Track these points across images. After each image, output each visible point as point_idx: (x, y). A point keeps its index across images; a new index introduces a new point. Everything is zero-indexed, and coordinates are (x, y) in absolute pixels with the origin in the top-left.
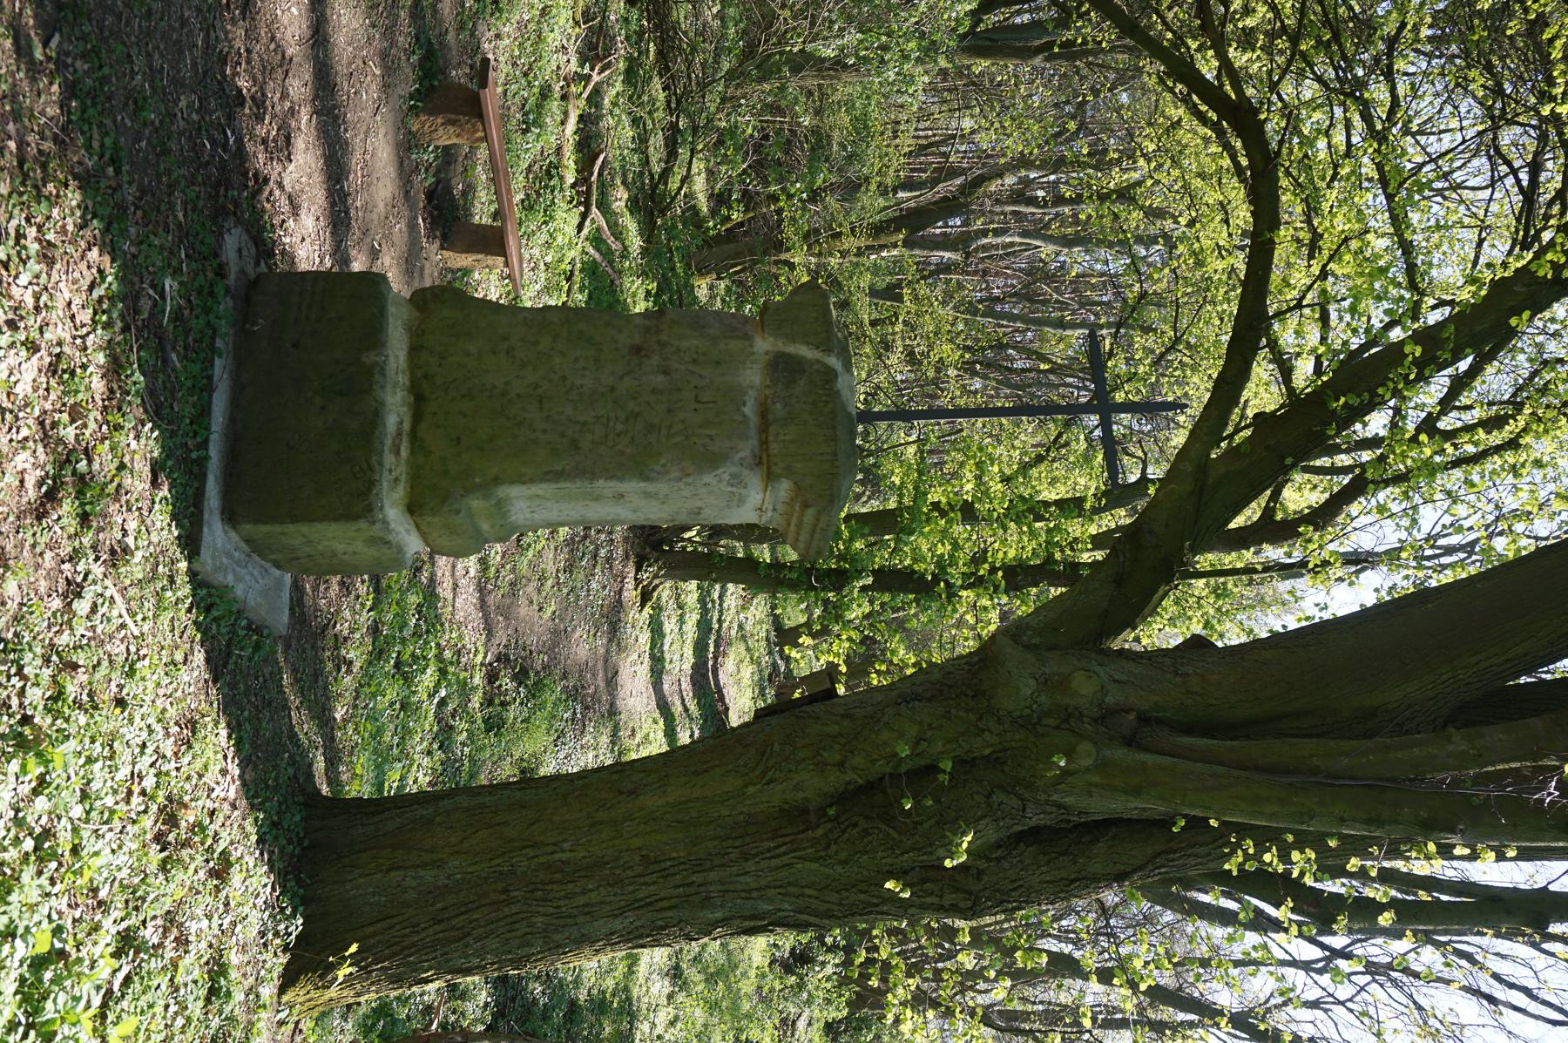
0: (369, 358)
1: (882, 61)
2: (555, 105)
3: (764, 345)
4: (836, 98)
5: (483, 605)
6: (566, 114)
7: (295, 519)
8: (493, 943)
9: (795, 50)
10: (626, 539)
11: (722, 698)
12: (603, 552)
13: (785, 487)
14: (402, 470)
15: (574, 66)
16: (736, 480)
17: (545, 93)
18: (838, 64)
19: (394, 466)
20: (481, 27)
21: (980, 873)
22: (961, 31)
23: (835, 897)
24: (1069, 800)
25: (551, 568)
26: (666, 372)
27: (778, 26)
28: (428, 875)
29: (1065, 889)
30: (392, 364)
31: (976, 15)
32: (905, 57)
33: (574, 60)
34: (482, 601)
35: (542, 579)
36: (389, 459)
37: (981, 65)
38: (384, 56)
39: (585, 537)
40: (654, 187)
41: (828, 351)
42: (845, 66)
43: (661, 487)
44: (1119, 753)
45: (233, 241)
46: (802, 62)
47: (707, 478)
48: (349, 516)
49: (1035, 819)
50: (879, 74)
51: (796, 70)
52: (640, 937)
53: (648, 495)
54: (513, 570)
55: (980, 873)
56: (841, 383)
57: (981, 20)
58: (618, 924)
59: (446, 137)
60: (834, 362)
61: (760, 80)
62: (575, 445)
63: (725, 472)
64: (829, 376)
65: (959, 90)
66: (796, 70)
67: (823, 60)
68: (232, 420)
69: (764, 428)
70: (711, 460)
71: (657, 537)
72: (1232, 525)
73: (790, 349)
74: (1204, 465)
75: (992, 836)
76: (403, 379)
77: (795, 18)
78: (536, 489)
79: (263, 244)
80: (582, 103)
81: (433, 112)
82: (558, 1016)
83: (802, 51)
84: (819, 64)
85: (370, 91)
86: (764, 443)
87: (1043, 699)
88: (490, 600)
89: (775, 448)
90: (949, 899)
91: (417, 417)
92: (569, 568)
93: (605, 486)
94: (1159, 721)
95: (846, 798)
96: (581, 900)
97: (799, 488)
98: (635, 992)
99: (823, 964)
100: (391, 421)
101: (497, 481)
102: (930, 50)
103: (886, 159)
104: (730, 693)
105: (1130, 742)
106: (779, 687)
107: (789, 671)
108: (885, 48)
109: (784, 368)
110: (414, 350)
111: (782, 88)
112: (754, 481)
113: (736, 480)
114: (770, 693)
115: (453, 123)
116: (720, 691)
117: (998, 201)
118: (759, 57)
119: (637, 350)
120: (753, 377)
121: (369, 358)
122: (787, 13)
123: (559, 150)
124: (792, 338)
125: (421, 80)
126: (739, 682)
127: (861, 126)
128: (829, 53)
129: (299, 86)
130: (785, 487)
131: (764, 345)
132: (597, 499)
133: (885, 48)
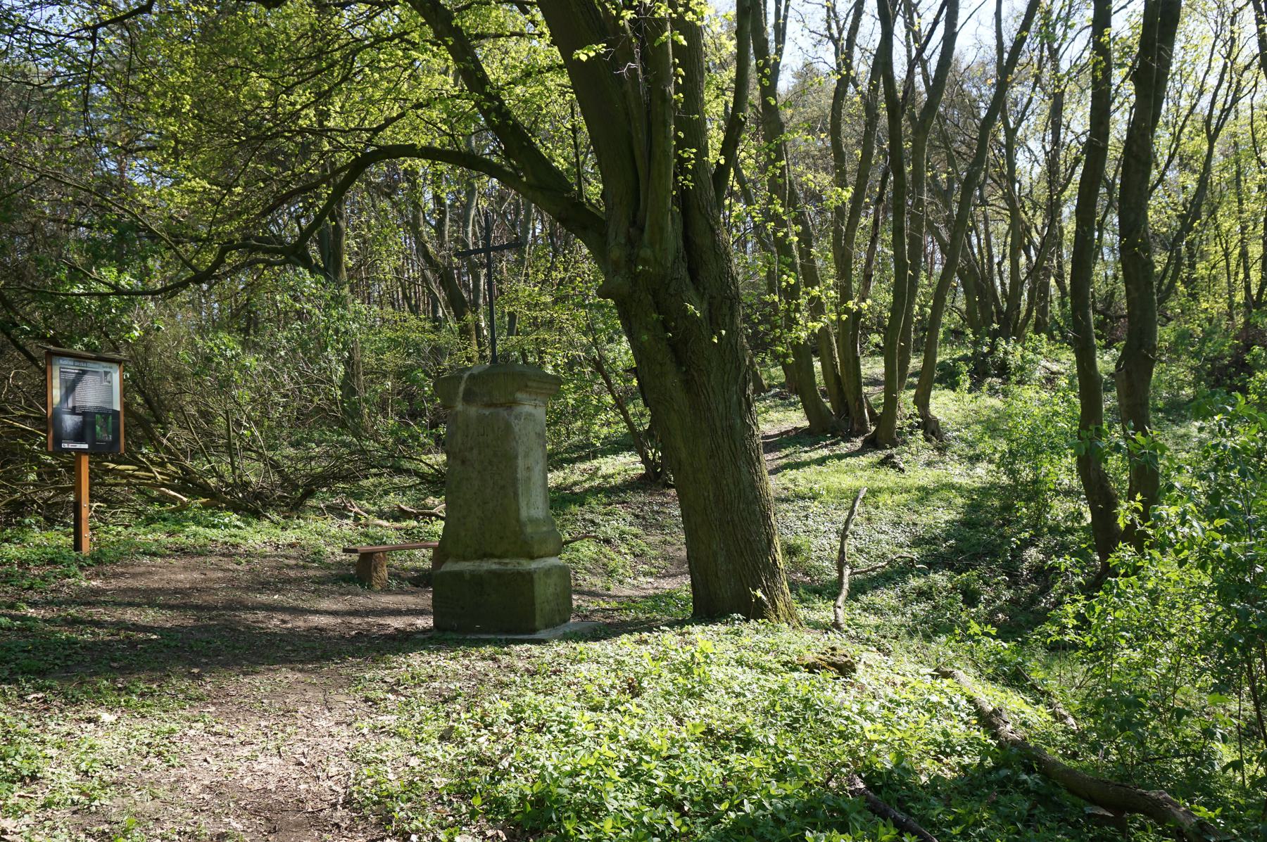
0: (467, 576)
1: (346, 332)
2: (371, 531)
3: (459, 406)
4: (373, 361)
5: (674, 576)
6: (377, 525)
7: (533, 604)
8: (754, 528)
9: (339, 392)
10: (651, 495)
11: (787, 432)
12: (656, 508)
13: (519, 395)
14: (514, 561)
15: (350, 522)
16: (518, 417)
17: (367, 536)
18: (349, 363)
19: (512, 565)
20: (328, 561)
21: (711, 297)
22: (323, 280)
23: (728, 366)
24: (670, 258)
25: (660, 538)
26: (472, 449)
27: (324, 404)
28: (721, 559)
29: (723, 256)
30: (471, 568)
31: (313, 270)
32: (342, 317)
33: (346, 521)
34: (670, 576)
35: (665, 542)
36: (510, 567)
37: (348, 261)
38: (342, 594)
39: (644, 518)
40: (429, 482)
41: (461, 378)
42: (351, 357)
43: (521, 450)
44: (646, 236)
45: (419, 636)
46: (348, 387)
47: (516, 429)
48: (532, 581)
49: (683, 272)
50: (355, 334)
51: (354, 392)
52: (751, 458)
53: (526, 456)
54: (655, 559)
55: (711, 297)
56: (475, 371)
57: (317, 265)
58: (744, 469)
59: (384, 573)
60: (466, 376)
61: (361, 417)
62: (503, 487)
63: (514, 422)
64: (472, 377)
65: (362, 281)
66: (354, 392)
67: (346, 373)
68: (494, 633)
69: (495, 405)
70: (508, 428)
71: (652, 475)
72: (685, 43)
73: (461, 395)
74: (529, 186)
75: (691, 293)
76: (477, 563)
77: (319, 394)
78: (523, 504)
79: (425, 631)
80: (371, 517)
81: (370, 578)
82: (967, 533)
83: (341, 388)
84: (349, 376)
85: (361, 600)
86: (501, 405)
87: (623, 272)
88: (672, 571)
89: (503, 400)
90: (725, 310)
91: (492, 556)
92: (662, 528)
93: (521, 474)
94: (635, 216)
95: (679, 362)
96: (732, 486)
97: (519, 390)
98: (977, 485)
99: (1006, 353)
100: (494, 567)
101: (518, 520)
102: (338, 301)
103: (415, 327)
104: (786, 426)
105: (642, 230)
106: (791, 392)
107: (781, 385)
108: (337, 331)
109: (469, 397)
110: (465, 559)
111: (366, 401)
112: (518, 409)
113: (518, 417)
114: (795, 398)
115: (376, 568)
116: (782, 434)
117: (441, 246)
118: (346, 417)
119: (463, 462)
120: (473, 411)
121: (467, 576)
122: (316, 399)
123: (397, 529)
124: (456, 394)
125: (354, 583)
126: (780, 421)
127: (394, 343)
128: (341, 368)
129: (356, 621)
130: (519, 395)
131: (459, 406)
132: (529, 478)
133: (337, 331)
